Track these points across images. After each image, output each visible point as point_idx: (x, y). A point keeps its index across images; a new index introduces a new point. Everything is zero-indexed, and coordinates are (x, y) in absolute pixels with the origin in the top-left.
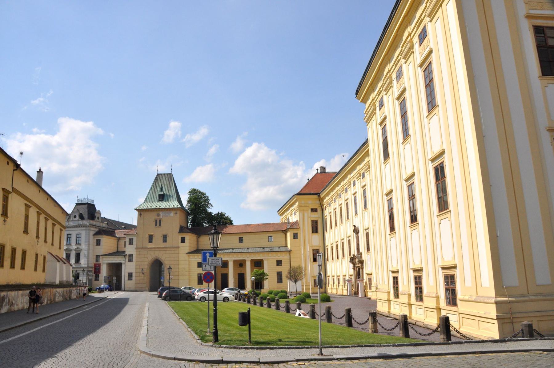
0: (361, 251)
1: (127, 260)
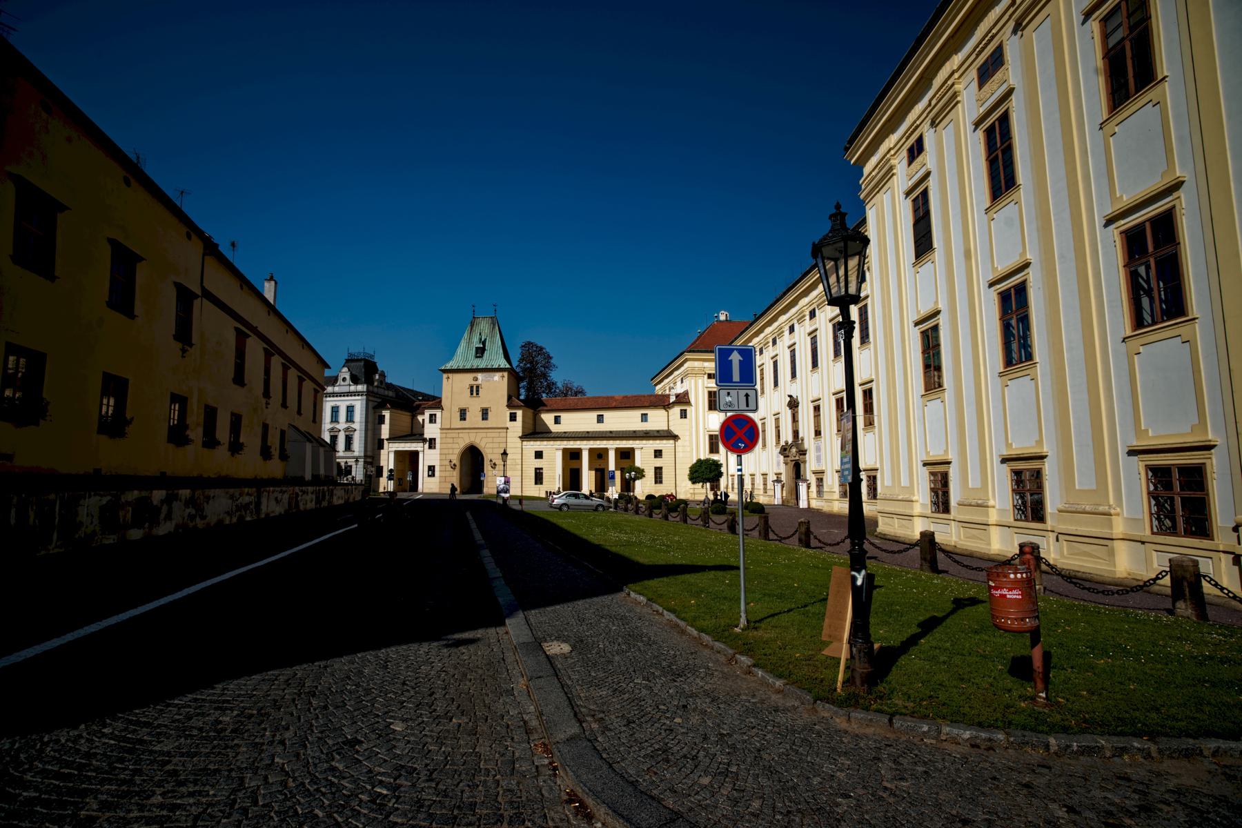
0: (801, 435)
1: (427, 445)
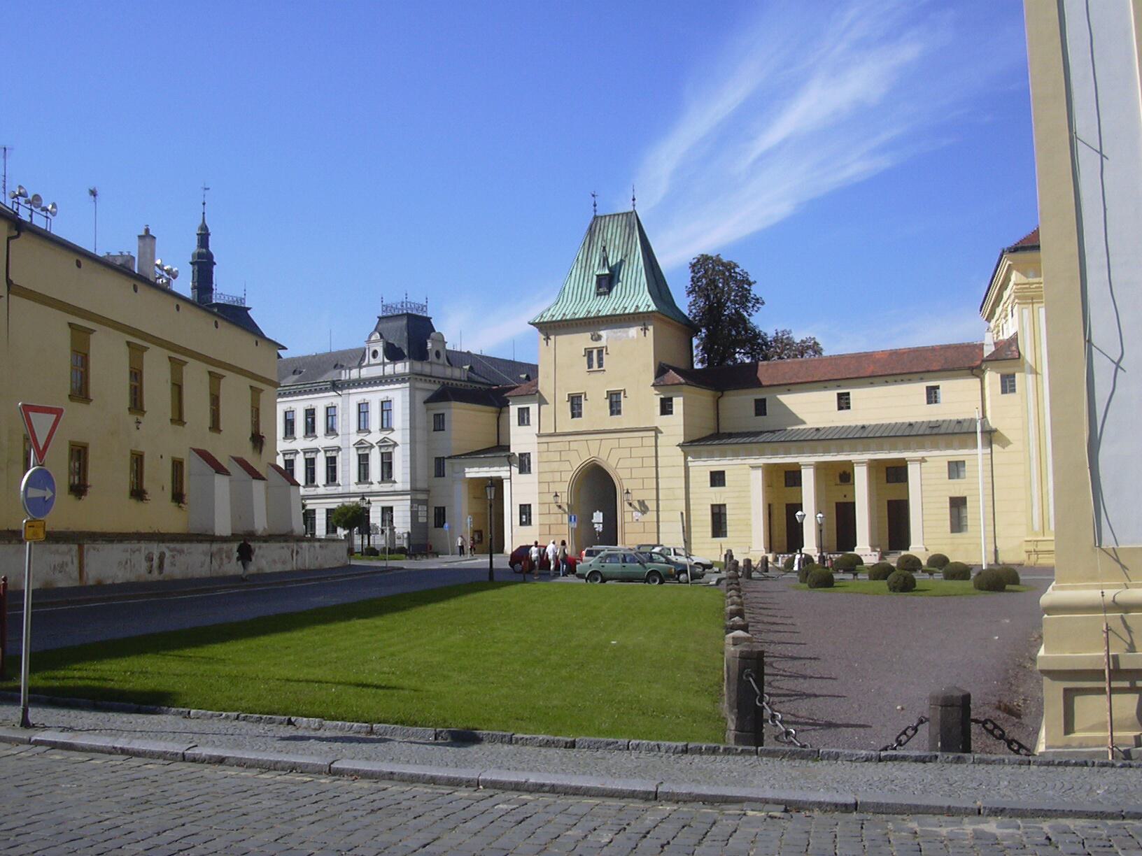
1: (515, 470)
